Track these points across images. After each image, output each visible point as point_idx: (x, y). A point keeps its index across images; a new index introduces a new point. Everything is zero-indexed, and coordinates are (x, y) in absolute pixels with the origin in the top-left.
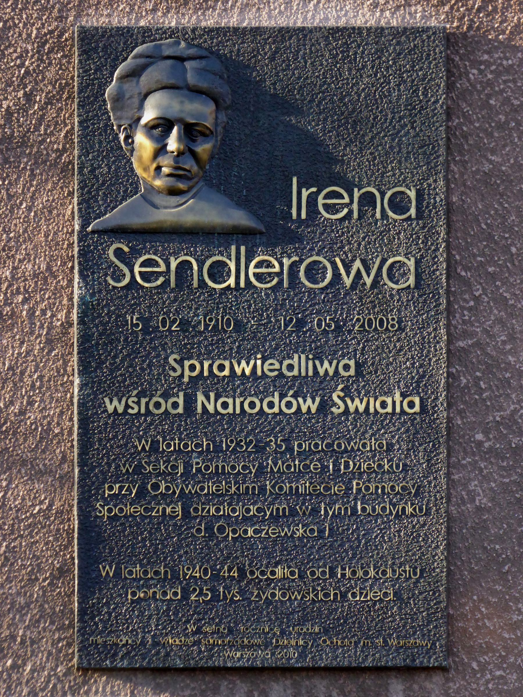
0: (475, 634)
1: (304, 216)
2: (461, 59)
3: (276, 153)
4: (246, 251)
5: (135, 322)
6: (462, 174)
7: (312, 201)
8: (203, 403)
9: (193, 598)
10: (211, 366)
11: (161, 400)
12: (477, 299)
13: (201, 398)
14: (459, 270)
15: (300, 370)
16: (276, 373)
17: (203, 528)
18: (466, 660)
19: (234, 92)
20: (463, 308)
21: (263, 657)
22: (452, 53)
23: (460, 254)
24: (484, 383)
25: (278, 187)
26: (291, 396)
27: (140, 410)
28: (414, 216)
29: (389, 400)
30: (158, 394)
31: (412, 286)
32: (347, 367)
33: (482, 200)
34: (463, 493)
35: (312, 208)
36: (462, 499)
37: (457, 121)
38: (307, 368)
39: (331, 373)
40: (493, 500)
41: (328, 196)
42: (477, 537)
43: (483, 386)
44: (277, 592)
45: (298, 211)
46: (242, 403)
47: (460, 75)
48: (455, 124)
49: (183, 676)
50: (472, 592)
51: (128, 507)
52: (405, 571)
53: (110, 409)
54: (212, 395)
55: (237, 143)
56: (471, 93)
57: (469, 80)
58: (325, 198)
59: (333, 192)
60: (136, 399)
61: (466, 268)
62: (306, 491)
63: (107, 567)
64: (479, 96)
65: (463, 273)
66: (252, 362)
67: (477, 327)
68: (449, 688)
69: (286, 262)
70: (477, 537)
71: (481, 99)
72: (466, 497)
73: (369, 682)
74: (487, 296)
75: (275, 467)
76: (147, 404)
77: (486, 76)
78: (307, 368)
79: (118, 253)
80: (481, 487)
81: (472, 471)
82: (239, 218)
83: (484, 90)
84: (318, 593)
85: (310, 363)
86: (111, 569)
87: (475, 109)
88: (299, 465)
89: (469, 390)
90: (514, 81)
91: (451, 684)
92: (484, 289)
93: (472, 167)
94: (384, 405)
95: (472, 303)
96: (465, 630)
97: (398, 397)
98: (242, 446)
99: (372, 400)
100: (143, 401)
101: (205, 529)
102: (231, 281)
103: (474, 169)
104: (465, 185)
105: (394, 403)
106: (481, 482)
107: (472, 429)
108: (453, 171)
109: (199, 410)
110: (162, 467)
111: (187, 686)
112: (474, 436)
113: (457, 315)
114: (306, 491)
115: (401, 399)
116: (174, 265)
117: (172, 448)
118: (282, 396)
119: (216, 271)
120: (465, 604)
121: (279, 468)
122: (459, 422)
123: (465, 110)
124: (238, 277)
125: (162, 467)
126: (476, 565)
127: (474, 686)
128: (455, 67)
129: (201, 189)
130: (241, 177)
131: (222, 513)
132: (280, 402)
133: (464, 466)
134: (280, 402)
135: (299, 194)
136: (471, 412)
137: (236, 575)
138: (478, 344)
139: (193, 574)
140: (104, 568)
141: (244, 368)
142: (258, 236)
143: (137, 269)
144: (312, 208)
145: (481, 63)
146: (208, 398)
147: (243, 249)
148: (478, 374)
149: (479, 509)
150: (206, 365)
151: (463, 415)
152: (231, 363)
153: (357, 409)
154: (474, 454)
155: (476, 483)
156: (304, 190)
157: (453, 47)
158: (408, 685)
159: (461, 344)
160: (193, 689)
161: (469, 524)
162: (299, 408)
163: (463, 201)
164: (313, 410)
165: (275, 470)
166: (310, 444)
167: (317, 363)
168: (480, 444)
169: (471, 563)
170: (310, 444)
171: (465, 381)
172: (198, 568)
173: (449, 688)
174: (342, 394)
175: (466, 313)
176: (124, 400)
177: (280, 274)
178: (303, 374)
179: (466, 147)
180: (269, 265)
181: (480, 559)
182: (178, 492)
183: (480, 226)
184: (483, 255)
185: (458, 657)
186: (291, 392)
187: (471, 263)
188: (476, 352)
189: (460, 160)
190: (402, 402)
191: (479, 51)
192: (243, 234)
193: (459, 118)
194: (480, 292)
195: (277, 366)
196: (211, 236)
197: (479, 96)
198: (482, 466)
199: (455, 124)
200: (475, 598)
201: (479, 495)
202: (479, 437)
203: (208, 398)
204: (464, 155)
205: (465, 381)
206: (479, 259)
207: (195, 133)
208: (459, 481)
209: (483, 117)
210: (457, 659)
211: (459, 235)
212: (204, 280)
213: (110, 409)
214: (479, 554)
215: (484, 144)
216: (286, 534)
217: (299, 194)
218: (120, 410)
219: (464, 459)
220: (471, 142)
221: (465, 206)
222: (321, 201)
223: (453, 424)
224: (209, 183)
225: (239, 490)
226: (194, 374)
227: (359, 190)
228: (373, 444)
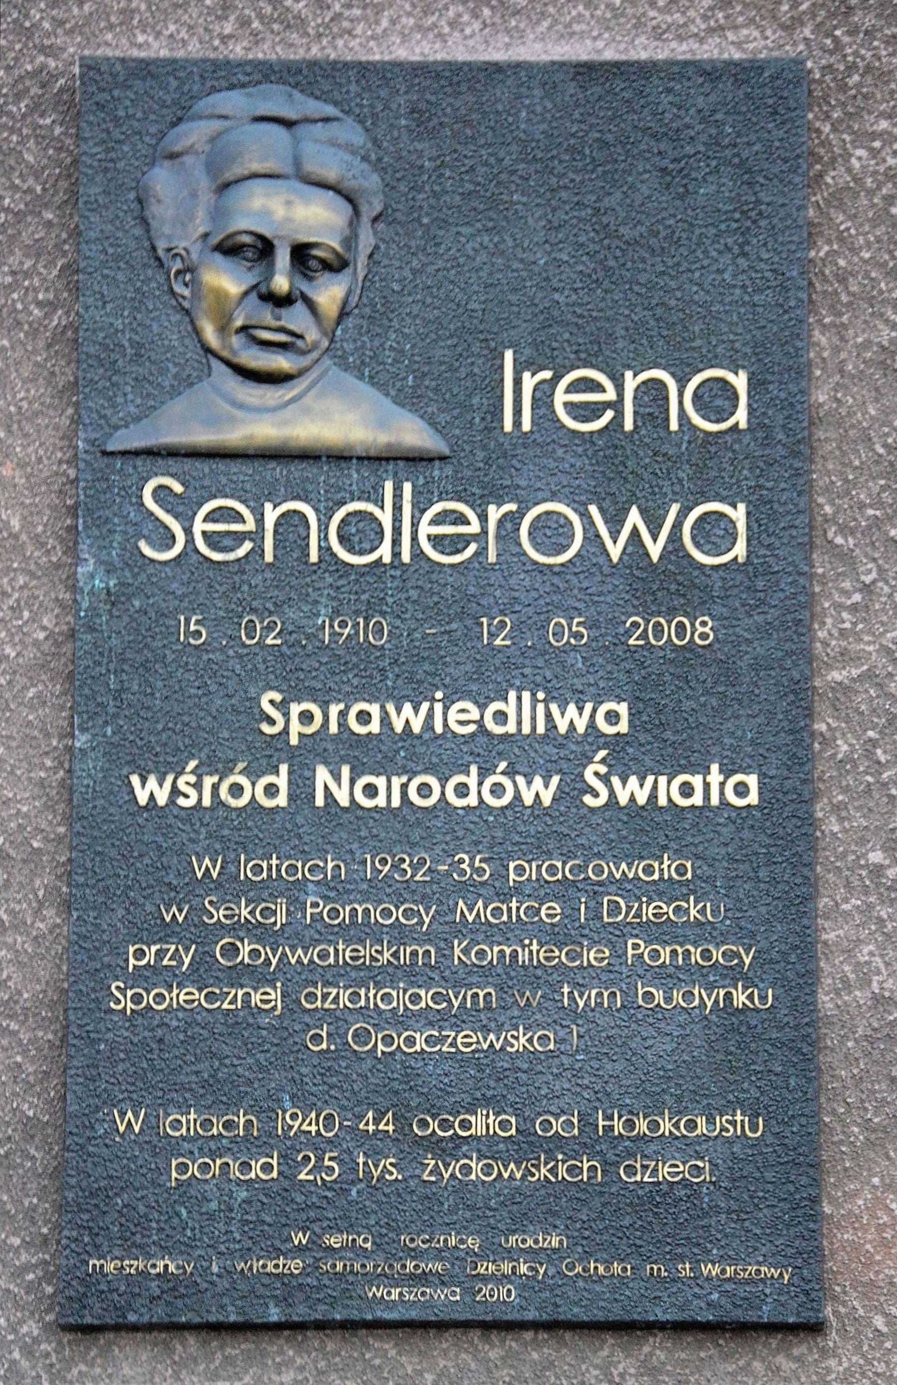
0: (878, 1258)
1: (526, 426)
2: (834, 129)
3: (472, 306)
4: (415, 493)
5: (193, 628)
6: (837, 350)
7: (543, 397)
8: (326, 787)
9: (302, 1177)
10: (343, 714)
11: (243, 781)
12: (867, 589)
13: (322, 775)
14: (830, 535)
15: (519, 723)
16: (472, 728)
17: (324, 1034)
18: (861, 1312)
19: (389, 187)
20: (839, 607)
21: (447, 1298)
22: (816, 118)
23: (831, 502)
24: (885, 752)
25: (476, 370)
26: (503, 773)
27: (200, 800)
28: (743, 425)
30: (237, 770)
31: (740, 560)
32: (612, 717)
33: (877, 400)
34: (847, 968)
35: (542, 412)
36: (845, 980)
37: (826, 248)
38: (534, 719)
39: (581, 728)
41: (572, 388)
42: (876, 1054)
43: (883, 759)
44: (473, 1165)
45: (517, 413)
46: (404, 787)
47: (833, 160)
48: (822, 254)
49: (282, 1341)
50: (870, 1170)
51: (175, 991)
52: (734, 1123)
53: (142, 798)
54: (346, 771)
55: (396, 287)
56: (856, 196)
57: (849, 170)
58: (568, 391)
59: (584, 379)
60: (193, 779)
61: (844, 530)
62: (531, 960)
63: (130, 1114)
64: (871, 200)
65: (839, 540)
66: (425, 706)
67: (869, 643)
68: (829, 1370)
69: (494, 513)
70: (876, 1054)
71: (874, 205)
72: (852, 976)
73: (661, 1355)
74: (887, 582)
75: (471, 910)
76: (215, 788)
77: (884, 161)
78: (534, 719)
79: (161, 493)
80: (882, 956)
81: (863, 925)
83: (879, 188)
84: (556, 1166)
85: (540, 707)
86: (137, 1117)
87: (861, 225)
88: (518, 909)
89: (855, 766)
91: (832, 1362)
92: (880, 569)
93: (857, 336)
94: (687, 790)
95: (857, 597)
96: (856, 1247)
97: (715, 777)
98: (405, 871)
99: (662, 780)
100: (208, 782)
101: (329, 1035)
102: (385, 552)
103: (860, 340)
104: (841, 371)
105: (707, 786)
106: (881, 947)
107: (863, 841)
108: (818, 344)
109: (320, 801)
110: (244, 913)
111: (288, 1363)
112: (864, 855)
113: (829, 621)
114: (531, 960)
115: (721, 778)
116: (271, 515)
117: (265, 875)
118: (483, 774)
119: (353, 530)
120: (856, 1194)
121: (478, 915)
122: (836, 829)
123: (842, 227)
124: (396, 542)
125: (244, 913)
126: (876, 1114)
127: (881, 1368)
128: (822, 144)
129: (326, 371)
130: (402, 351)
131: (363, 1003)
132: (480, 784)
133: (847, 914)
134: (480, 784)
135: (518, 382)
136: (858, 808)
137: (391, 1128)
138: (869, 676)
139: (305, 1127)
140: (123, 1114)
141: (408, 717)
142: (437, 463)
143: (199, 526)
144: (542, 412)
145: (874, 136)
146: (337, 778)
147: (407, 487)
148: (871, 734)
149: (878, 999)
150: (334, 710)
151: (844, 814)
152: (383, 707)
153: (632, 799)
154: (866, 891)
155: (871, 947)
156: (526, 375)
157: (820, 106)
158: (741, 1363)
159: (836, 675)
160: (302, 1369)
161: (860, 1031)
162: (518, 796)
163: (838, 401)
164: (547, 800)
165: (470, 919)
166: (539, 867)
167: (554, 708)
168: (877, 871)
169: (866, 1109)
170: (539, 867)
171: (845, 748)
172: (313, 1115)
173: (829, 1370)
174: (603, 769)
175: (845, 615)
176: (170, 779)
178: (526, 729)
179: (844, 298)
181: (884, 1102)
182: (274, 962)
183: (873, 450)
184: (879, 504)
185: (844, 1304)
186: (503, 765)
187: (855, 520)
188: (866, 691)
189: (833, 325)
190: (722, 785)
191: (870, 113)
192: (407, 459)
193: (829, 242)
194: (874, 575)
195: (475, 714)
196: (343, 465)
197: (871, 200)
198: (884, 914)
199: (822, 254)
200: (876, 1181)
201: (878, 972)
202: (877, 857)
203: (337, 778)
204: (840, 314)
205: (845, 748)
206: (871, 512)
207: (313, 263)
208: (836, 944)
209: (878, 240)
210: (842, 1310)
211: (831, 467)
212: (329, 548)
213: (142, 798)
214: (881, 1091)
215: (881, 292)
216: (491, 1045)
217: (518, 382)
218: (162, 799)
219: (846, 900)
220: (854, 289)
221: (843, 411)
222: (560, 397)
223: (823, 832)
224: (344, 364)
225: (398, 959)
226: (309, 730)
227: (635, 375)
228: (371, 995)
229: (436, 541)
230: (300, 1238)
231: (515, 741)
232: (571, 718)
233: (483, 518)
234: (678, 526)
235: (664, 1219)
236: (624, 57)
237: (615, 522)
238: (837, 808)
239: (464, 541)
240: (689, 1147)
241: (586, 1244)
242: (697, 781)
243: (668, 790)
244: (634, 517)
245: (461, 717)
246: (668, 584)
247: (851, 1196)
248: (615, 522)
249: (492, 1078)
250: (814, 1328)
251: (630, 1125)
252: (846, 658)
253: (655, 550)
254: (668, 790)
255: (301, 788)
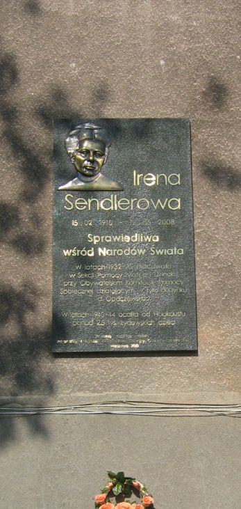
29: (172, 250)
40: (211, 287)
45: (137, 182)
69: (132, 201)
82: (113, 185)
90: (215, 138)
94: (170, 252)
97: (175, 249)
135: (136, 176)
141: (116, 238)
143: (76, 203)
149: (207, 291)
168: (206, 267)
177: (87, 206)
180: (127, 202)
217: (136, 176)
222: (144, 179)
229: (121, 206)
230: (98, 336)
231: (136, 241)
232: (148, 239)
233: (130, 201)
234: (167, 202)
235: (167, 332)
236: (199, 305)
237: (156, 202)
238: (198, 255)
239: (127, 206)
240: (172, 319)
241: (152, 337)
242: (172, 250)
243: (166, 252)
244: (159, 201)
245: (128, 239)
246: (166, 213)
247: (202, 327)
248: (156, 202)
249: (134, 307)
250: (194, 353)
251: (160, 314)
252: (199, 227)
253: (163, 207)
254: (166, 252)
255: (96, 252)
